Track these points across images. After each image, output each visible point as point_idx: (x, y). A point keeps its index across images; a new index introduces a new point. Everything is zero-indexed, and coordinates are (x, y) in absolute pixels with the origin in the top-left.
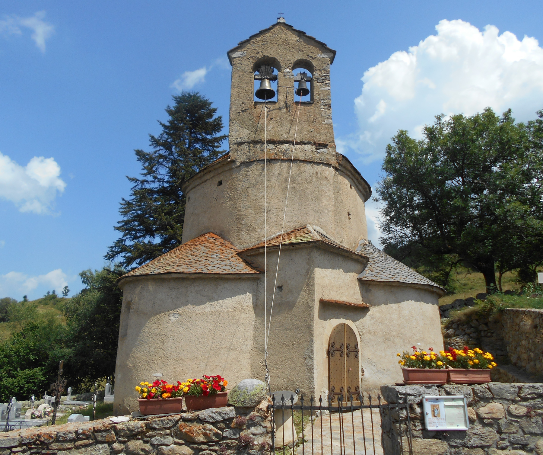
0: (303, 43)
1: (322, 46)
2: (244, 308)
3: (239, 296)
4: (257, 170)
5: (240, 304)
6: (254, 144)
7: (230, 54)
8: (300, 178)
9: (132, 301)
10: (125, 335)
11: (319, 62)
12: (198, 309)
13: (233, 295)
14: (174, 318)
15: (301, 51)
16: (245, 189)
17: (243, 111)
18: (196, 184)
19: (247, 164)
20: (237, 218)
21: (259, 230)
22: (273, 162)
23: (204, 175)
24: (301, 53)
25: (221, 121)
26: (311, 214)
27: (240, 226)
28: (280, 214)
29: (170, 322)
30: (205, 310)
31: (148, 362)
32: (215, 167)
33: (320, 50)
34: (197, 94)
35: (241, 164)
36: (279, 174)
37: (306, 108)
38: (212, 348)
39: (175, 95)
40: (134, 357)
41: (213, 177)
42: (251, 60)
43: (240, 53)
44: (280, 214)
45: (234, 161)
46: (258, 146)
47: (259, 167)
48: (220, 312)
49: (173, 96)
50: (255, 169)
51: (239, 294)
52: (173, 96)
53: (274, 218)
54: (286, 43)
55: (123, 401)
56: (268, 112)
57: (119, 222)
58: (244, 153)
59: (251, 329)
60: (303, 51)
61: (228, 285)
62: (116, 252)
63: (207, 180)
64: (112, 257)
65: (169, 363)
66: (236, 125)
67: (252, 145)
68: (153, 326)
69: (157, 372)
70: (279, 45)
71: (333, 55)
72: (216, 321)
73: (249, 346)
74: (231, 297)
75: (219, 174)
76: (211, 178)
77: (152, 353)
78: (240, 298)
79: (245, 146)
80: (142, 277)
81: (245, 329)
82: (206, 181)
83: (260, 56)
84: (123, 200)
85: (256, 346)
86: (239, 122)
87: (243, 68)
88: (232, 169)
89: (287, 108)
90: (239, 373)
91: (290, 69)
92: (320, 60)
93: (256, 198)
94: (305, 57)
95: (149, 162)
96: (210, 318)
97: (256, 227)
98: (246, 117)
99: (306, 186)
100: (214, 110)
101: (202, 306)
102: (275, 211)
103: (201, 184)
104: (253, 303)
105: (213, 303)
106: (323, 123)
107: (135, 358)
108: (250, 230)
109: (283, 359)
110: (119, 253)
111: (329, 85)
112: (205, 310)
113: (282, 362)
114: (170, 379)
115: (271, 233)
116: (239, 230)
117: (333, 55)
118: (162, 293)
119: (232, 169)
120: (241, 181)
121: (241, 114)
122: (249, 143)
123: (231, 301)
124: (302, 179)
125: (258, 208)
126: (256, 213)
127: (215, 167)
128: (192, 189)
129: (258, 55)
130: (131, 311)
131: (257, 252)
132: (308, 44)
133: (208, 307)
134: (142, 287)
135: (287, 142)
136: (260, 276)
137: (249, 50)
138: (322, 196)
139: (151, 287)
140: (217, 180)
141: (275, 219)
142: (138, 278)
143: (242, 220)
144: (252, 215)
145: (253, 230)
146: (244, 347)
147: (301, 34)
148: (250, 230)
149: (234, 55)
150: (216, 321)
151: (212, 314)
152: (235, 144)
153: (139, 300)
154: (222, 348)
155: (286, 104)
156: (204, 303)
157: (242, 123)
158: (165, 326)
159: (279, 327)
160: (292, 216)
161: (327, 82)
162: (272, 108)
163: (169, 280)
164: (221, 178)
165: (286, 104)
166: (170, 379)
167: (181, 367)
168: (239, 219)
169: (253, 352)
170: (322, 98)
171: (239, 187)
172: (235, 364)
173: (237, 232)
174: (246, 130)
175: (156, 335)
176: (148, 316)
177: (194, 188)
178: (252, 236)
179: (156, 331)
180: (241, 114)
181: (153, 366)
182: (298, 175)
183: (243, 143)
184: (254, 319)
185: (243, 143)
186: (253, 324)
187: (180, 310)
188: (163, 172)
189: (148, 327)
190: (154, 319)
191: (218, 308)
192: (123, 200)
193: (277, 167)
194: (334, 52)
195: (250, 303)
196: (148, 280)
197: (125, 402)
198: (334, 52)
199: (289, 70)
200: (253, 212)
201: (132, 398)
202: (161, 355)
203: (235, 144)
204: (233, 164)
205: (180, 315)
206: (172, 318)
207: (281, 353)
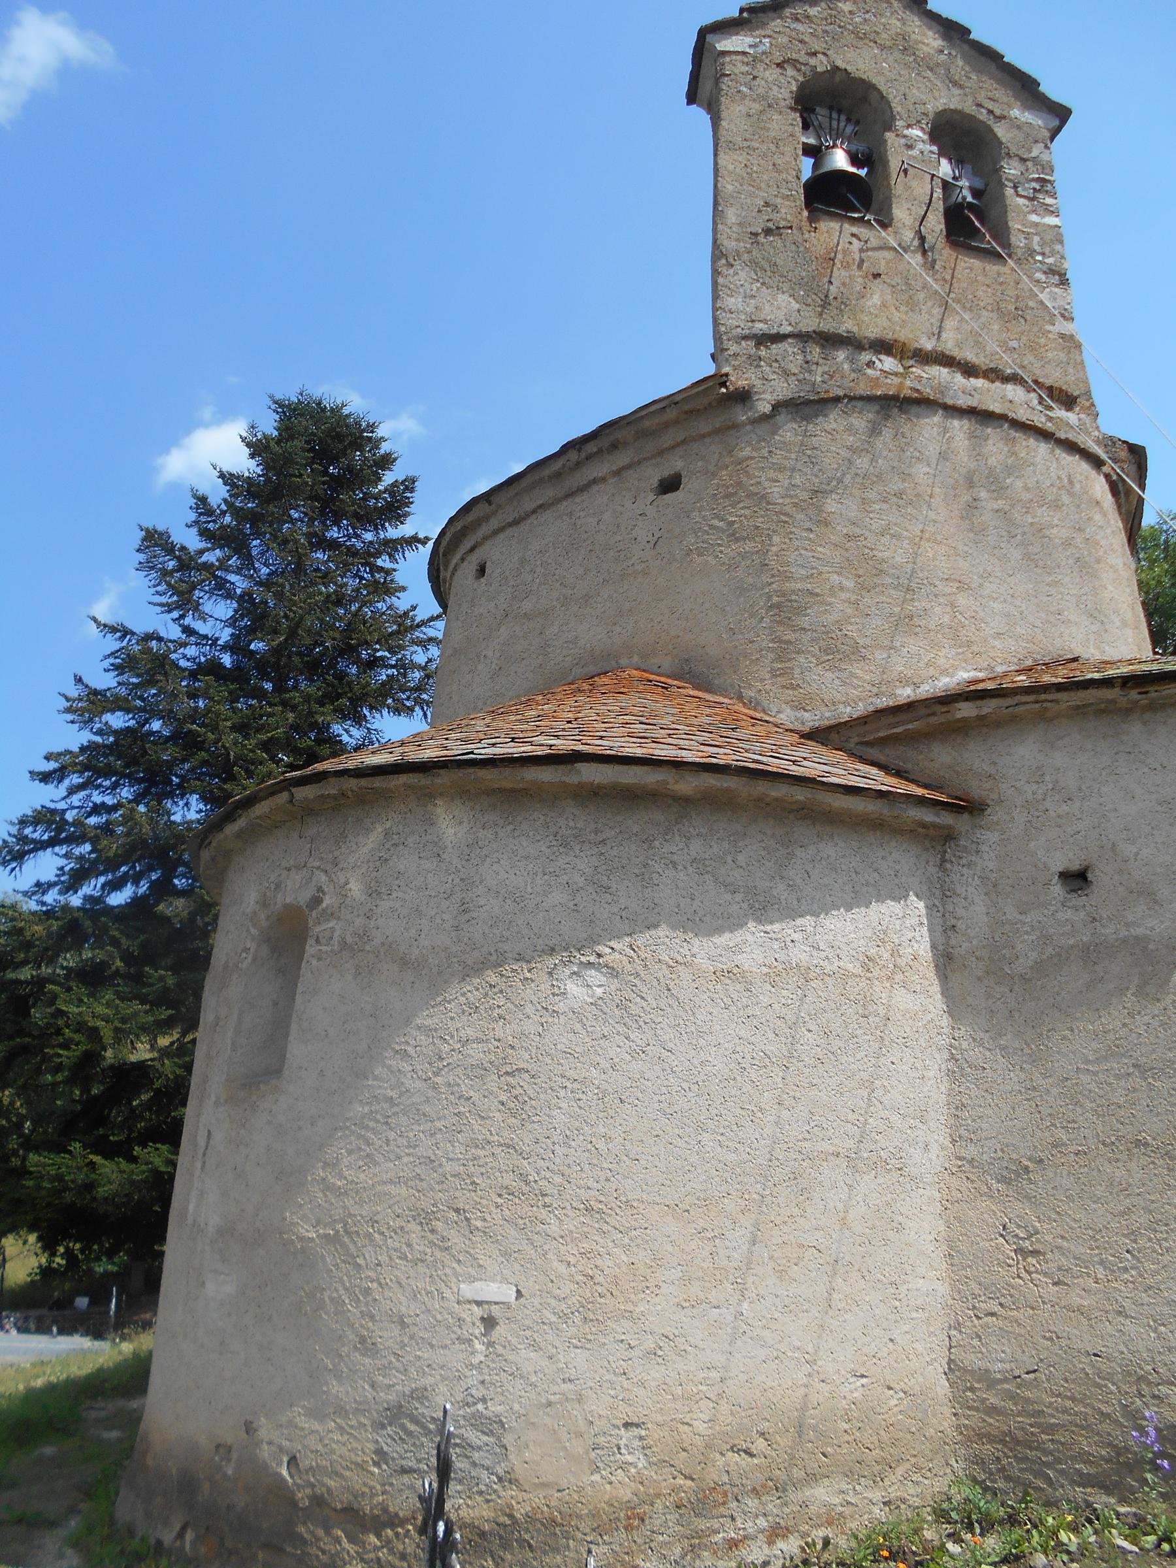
0: (960, 63)
1: (1025, 86)
2: (902, 962)
3: (883, 908)
4: (850, 429)
5: (873, 942)
6: (823, 347)
7: (710, 38)
8: (1019, 484)
9: (316, 901)
10: (265, 1072)
11: (1016, 132)
12: (705, 951)
13: (857, 898)
14: (580, 990)
15: (956, 84)
16: (804, 495)
17: (768, 232)
18: (529, 505)
19: (806, 406)
20: (778, 606)
21: (880, 655)
22: (915, 409)
23: (578, 465)
24: (956, 91)
25: (412, 490)
26: (1072, 618)
27: (790, 636)
28: (962, 600)
29: (561, 1007)
30: (740, 959)
31: (425, 1219)
32: (647, 423)
33: (1016, 98)
34: (343, 405)
35: (777, 407)
36: (943, 456)
37: (988, 267)
38: (778, 1153)
39: (279, 396)
40: (328, 1188)
41: (628, 467)
42: (790, 72)
43: (749, 40)
44: (962, 600)
45: (743, 397)
46: (841, 355)
47: (860, 421)
48: (805, 973)
49: (271, 397)
50: (838, 431)
51: (881, 899)
52: (271, 397)
53: (939, 614)
54: (906, 47)
55: (249, 1428)
56: (861, 251)
57: (48, 758)
58: (786, 373)
59: (936, 1064)
60: (961, 87)
61: (836, 850)
62: (34, 841)
63: (594, 481)
64: (14, 859)
65: (554, 1228)
66: (742, 275)
67: (816, 351)
68: (458, 1024)
69: (480, 1273)
70: (882, 48)
71: (1057, 123)
72: (790, 1017)
73: (934, 1149)
74: (849, 908)
75: (661, 453)
76: (618, 473)
77: (448, 1167)
78: (885, 911)
79: (789, 348)
80: (403, 779)
81: (914, 1068)
82: (582, 489)
83: (821, 64)
84: (79, 680)
85: (971, 1151)
86: (754, 264)
87: (761, 91)
88: (735, 426)
89: (924, 252)
90: (903, 1289)
91: (922, 129)
92: (1019, 127)
93: (858, 531)
94: (969, 108)
95: (179, 575)
96: (765, 1000)
97: (868, 641)
98: (779, 251)
99: (1043, 514)
100: (387, 461)
101: (725, 939)
102: (942, 587)
103: (557, 501)
104: (934, 947)
105: (776, 927)
106: (1049, 327)
107: (340, 1193)
108: (838, 651)
109: (1140, 1219)
110: (41, 846)
111: (1055, 213)
112: (740, 959)
113: (1133, 1235)
114: (563, 1317)
115: (932, 671)
116: (784, 652)
117: (1057, 123)
118: (519, 865)
119: (735, 426)
120: (781, 469)
121: (761, 239)
122: (803, 337)
123: (850, 927)
124: (1027, 489)
125: (870, 574)
126: (863, 588)
127: (647, 423)
128: (496, 532)
129: (813, 61)
130: (311, 949)
131: (942, 719)
132: (980, 72)
133: (752, 945)
134: (387, 834)
135: (946, 361)
136: (961, 823)
137: (783, 40)
138: (1098, 561)
139: (451, 825)
140: (654, 474)
141: (946, 619)
142: (377, 782)
143: (801, 611)
144: (843, 596)
145: (856, 653)
146: (916, 1154)
147: (953, 31)
148: (838, 651)
149: (726, 44)
150: (790, 1017)
151: (773, 979)
152: (745, 338)
153: (373, 892)
154: (825, 1156)
155: (922, 239)
156: (733, 923)
157: (768, 272)
158: (530, 1027)
159: (1097, 1061)
160: (1008, 615)
161: (1049, 201)
162: (874, 242)
163: (549, 797)
164: (675, 464)
165: (922, 239)
166: (563, 1317)
167: (626, 1248)
168: (785, 609)
169: (954, 1182)
170: (1037, 248)
171: (776, 491)
172: (886, 1242)
173: (779, 659)
174: (786, 297)
175: (480, 1071)
176: (433, 973)
177: (516, 522)
178: (852, 674)
179: (475, 1052)
180: (761, 239)
181: (456, 1240)
182: (1009, 470)
183: (778, 338)
184: (945, 1021)
185: (778, 338)
186: (944, 1041)
187: (616, 951)
188: (217, 616)
189: (428, 1031)
190: (471, 991)
191: (800, 954)
192: (79, 680)
193: (929, 429)
194: (1061, 114)
195: (923, 947)
196: (429, 796)
197: (263, 1433)
198: (1061, 114)
199: (920, 134)
200: (849, 584)
201: (311, 1414)
202: (508, 1179)
203: (745, 338)
204: (738, 408)
205: (613, 972)
206: (573, 988)
207: (1125, 1189)
